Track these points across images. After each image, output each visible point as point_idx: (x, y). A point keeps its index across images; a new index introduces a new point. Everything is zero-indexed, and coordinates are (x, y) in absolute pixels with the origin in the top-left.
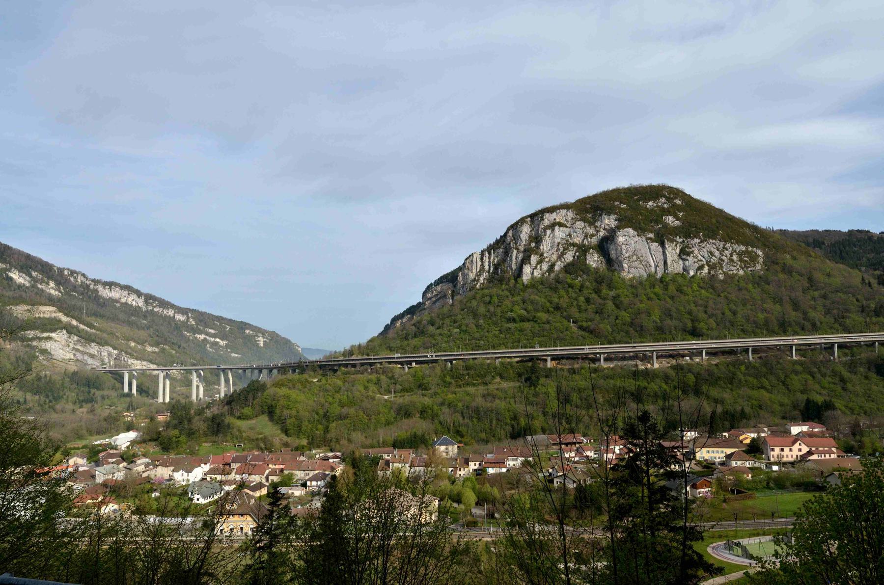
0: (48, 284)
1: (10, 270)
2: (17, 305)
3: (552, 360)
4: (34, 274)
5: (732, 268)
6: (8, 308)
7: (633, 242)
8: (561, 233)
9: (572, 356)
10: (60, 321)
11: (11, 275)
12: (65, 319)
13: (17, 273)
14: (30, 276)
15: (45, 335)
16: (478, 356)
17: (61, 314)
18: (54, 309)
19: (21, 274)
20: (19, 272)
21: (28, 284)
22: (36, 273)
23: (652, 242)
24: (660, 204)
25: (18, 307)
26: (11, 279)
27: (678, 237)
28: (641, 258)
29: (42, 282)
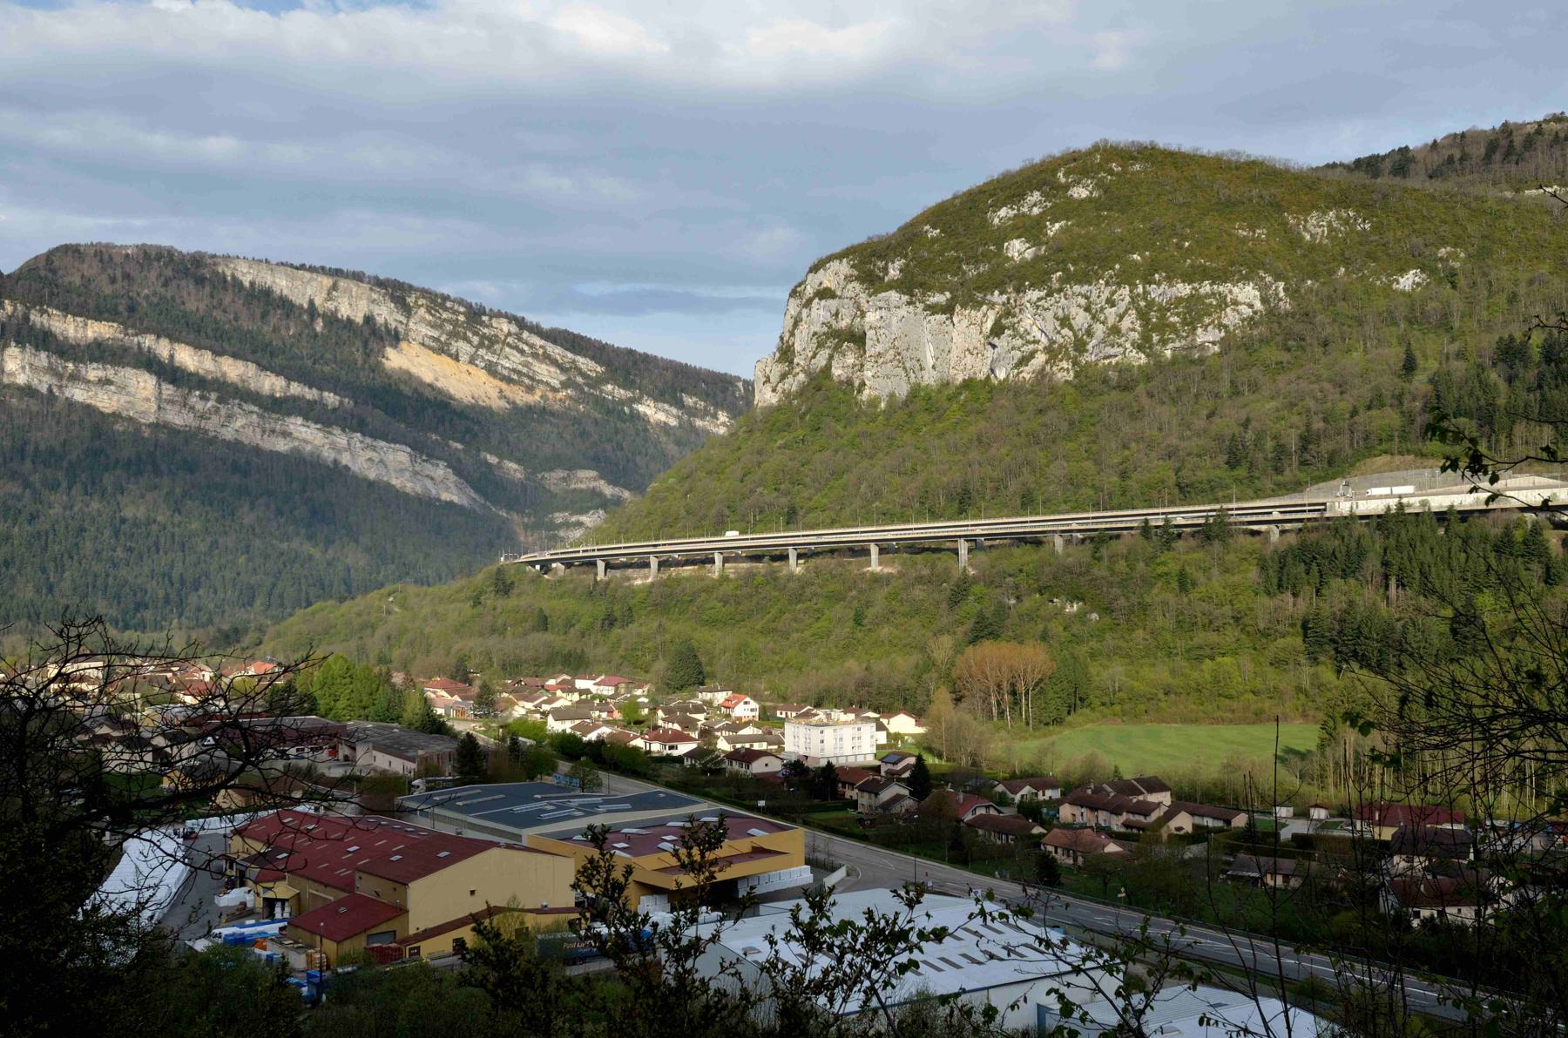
0: (715, 416)
1: (639, 401)
2: (551, 470)
3: (799, 556)
4: (689, 401)
5: (1112, 351)
6: (539, 476)
7: (894, 320)
8: (821, 312)
9: (927, 544)
10: (599, 494)
11: (641, 408)
12: (608, 490)
13: (652, 404)
14: (679, 404)
15: (574, 519)
16: (1263, 528)
17: (602, 482)
18: (593, 473)
19: (660, 405)
20: (656, 400)
21: (673, 422)
22: (694, 399)
23: (933, 314)
24: (1025, 209)
25: (553, 474)
26: (643, 419)
27: (996, 293)
28: (904, 353)
29: (704, 414)
